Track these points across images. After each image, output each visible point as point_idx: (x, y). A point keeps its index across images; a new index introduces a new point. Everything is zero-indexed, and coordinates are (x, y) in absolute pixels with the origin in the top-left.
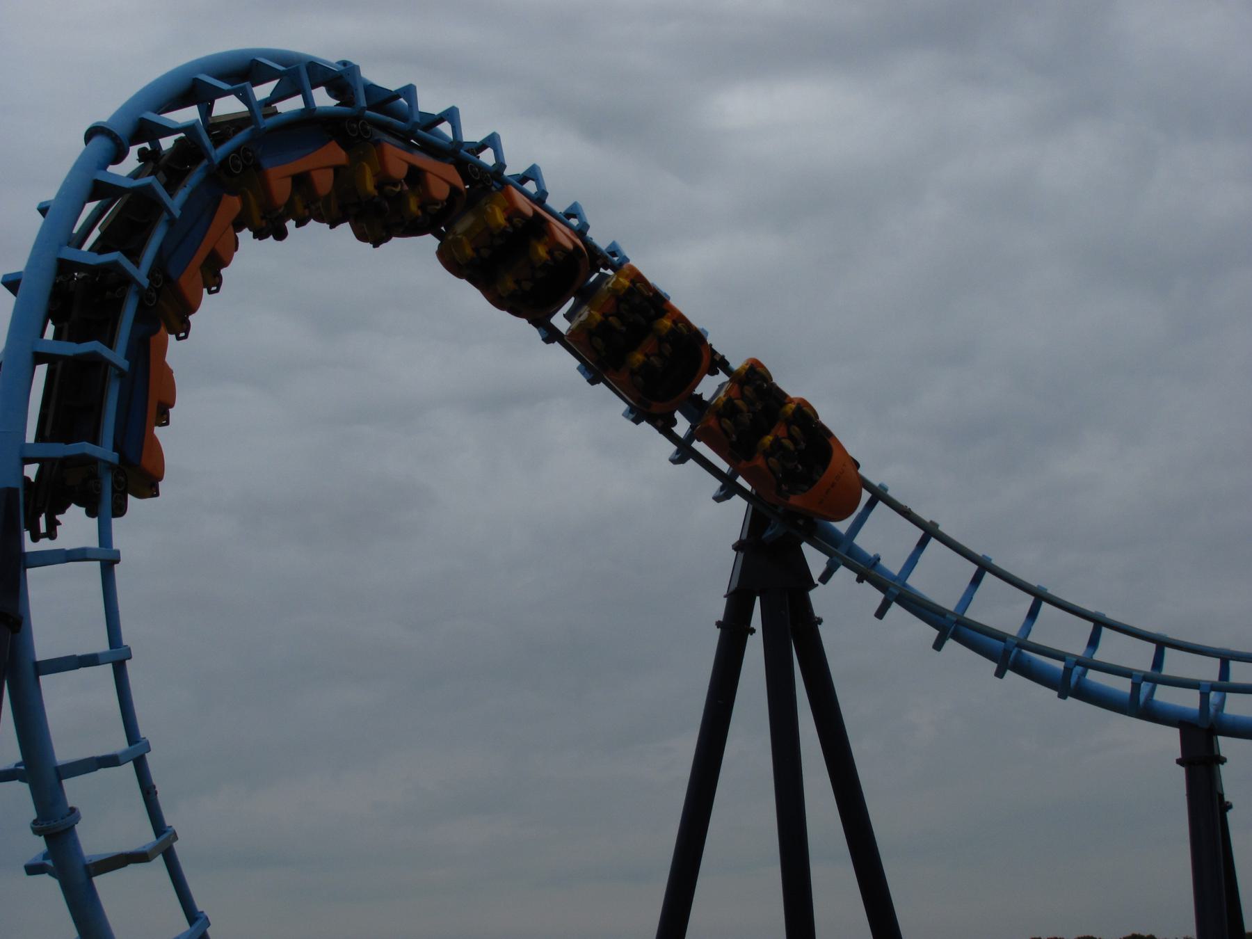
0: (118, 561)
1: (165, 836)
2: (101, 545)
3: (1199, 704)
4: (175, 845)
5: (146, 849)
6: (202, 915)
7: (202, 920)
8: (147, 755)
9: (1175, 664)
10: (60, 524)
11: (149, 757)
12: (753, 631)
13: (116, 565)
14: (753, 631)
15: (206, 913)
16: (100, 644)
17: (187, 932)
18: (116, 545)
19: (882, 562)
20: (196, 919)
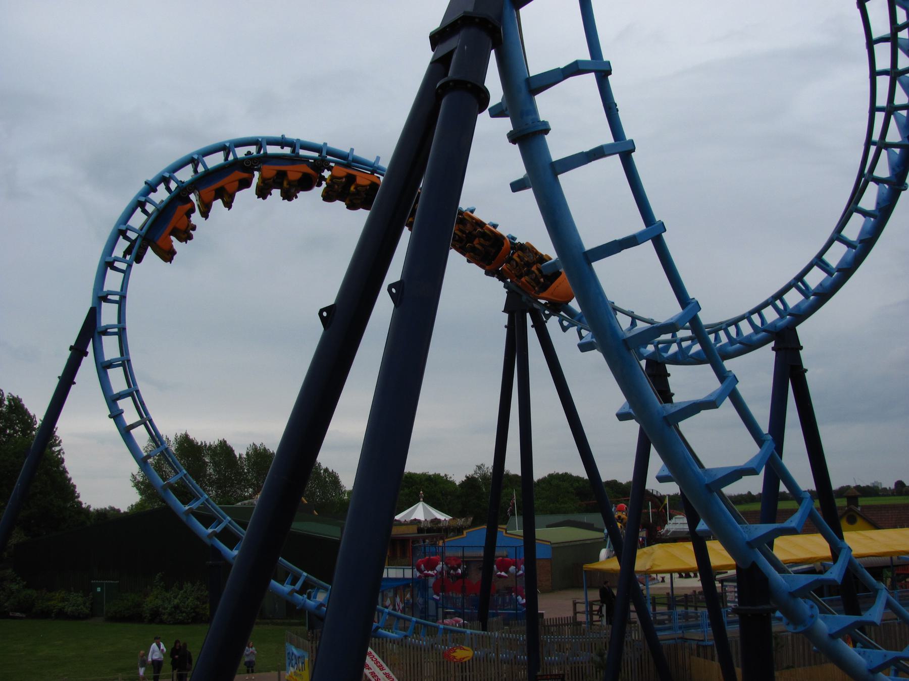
0: (633, 150)
1: (690, 306)
2: (615, 140)
3: (288, 148)
4: (738, 386)
5: (712, 398)
6: (730, 375)
7: (693, 304)
8: (699, 314)
9: (881, 101)
10: (229, 210)
11: (738, 387)
12: (282, 148)
13: (633, 154)
14: (282, 148)
15: (734, 372)
16: (638, 226)
17: (758, 454)
18: (628, 136)
19: (548, 138)
20: (688, 304)
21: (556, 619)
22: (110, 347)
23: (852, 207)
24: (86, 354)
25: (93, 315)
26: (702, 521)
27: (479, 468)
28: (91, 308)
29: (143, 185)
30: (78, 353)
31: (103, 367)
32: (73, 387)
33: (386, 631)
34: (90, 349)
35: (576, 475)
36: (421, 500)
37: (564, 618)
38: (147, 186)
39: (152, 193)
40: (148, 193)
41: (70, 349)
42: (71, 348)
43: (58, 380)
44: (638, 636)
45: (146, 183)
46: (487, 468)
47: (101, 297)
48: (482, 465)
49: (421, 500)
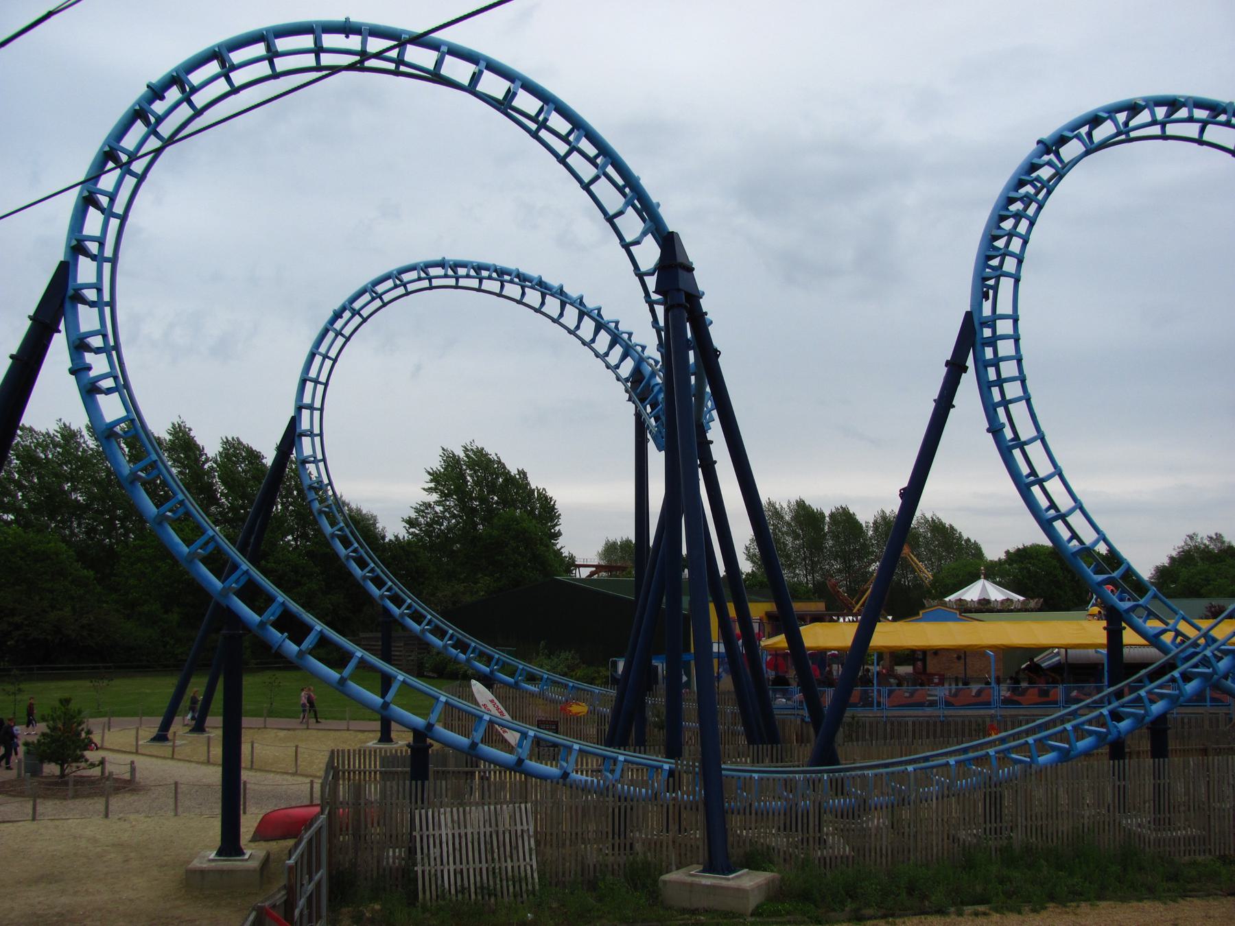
21: (349, 751)
22: (88, 319)
23: (436, 77)
24: (965, 369)
25: (64, 272)
26: (1173, 621)
27: (1191, 538)
28: (62, 263)
29: (1034, 146)
30: (955, 368)
31: (79, 346)
32: (952, 410)
33: (541, 763)
34: (970, 362)
35: (1030, 544)
36: (982, 576)
37: (343, 751)
38: (150, 92)
39: (158, 102)
40: (151, 102)
41: (946, 366)
42: (948, 363)
43: (933, 404)
44: (370, 788)
45: (148, 86)
46: (1202, 538)
47: (77, 248)
48: (1194, 534)
49: (982, 576)
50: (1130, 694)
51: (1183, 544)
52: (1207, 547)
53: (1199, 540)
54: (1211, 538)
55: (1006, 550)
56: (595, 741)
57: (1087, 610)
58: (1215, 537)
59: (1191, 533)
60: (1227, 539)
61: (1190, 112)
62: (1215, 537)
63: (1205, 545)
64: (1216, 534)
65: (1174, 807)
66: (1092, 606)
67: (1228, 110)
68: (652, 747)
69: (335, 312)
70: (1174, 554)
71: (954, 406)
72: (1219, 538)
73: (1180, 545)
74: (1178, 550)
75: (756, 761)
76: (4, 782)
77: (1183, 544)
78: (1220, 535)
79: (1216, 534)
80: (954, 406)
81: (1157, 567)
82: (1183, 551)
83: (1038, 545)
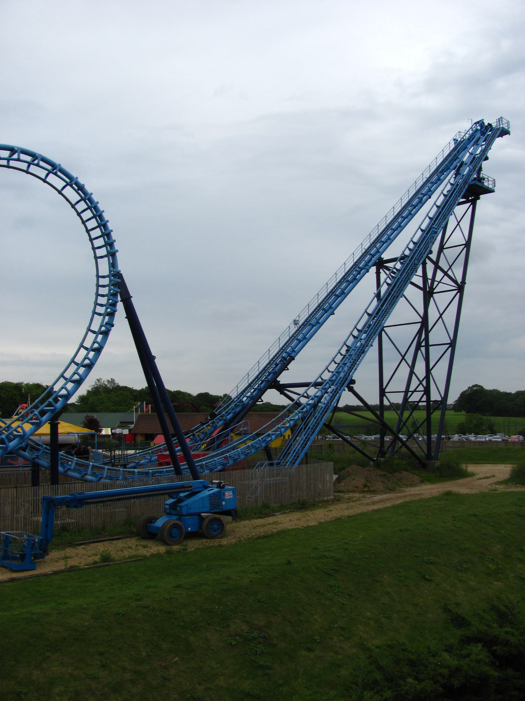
27: (98, 380)
48: (100, 379)
50: (202, 457)
51: (94, 384)
52: (106, 386)
53: (103, 382)
54: (109, 381)
55: (111, 378)
56: (191, 477)
57: (12, 418)
58: (110, 380)
59: (98, 378)
60: (116, 382)
61: (19, 156)
62: (110, 380)
63: (105, 384)
64: (111, 379)
65: (29, 525)
66: (15, 416)
67: (39, 158)
68: (28, 488)
69: (83, 185)
70: (90, 389)
71: (132, 297)
72: (113, 381)
73: (93, 385)
74: (92, 387)
75: (57, 494)
76: (523, 484)
77: (94, 384)
78: (114, 380)
79: (111, 379)
80: (132, 297)
81: (80, 396)
82: (94, 388)
83: (8, 382)
